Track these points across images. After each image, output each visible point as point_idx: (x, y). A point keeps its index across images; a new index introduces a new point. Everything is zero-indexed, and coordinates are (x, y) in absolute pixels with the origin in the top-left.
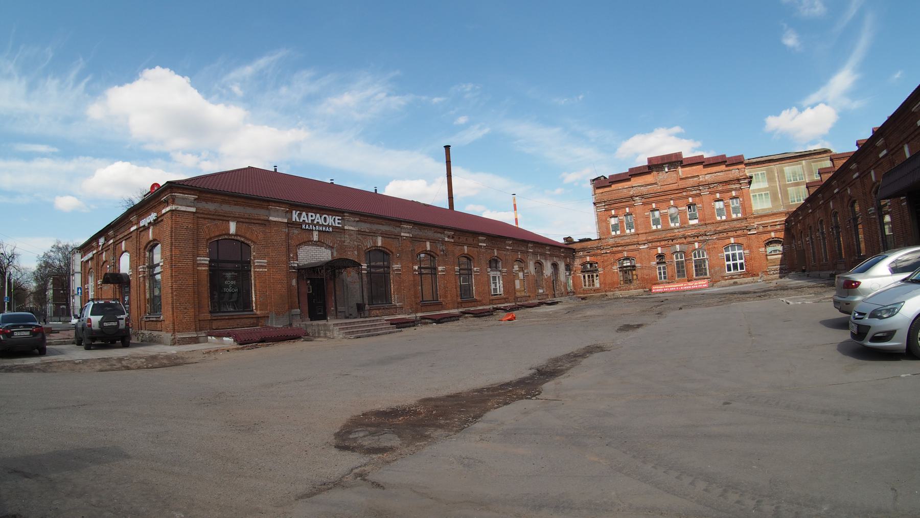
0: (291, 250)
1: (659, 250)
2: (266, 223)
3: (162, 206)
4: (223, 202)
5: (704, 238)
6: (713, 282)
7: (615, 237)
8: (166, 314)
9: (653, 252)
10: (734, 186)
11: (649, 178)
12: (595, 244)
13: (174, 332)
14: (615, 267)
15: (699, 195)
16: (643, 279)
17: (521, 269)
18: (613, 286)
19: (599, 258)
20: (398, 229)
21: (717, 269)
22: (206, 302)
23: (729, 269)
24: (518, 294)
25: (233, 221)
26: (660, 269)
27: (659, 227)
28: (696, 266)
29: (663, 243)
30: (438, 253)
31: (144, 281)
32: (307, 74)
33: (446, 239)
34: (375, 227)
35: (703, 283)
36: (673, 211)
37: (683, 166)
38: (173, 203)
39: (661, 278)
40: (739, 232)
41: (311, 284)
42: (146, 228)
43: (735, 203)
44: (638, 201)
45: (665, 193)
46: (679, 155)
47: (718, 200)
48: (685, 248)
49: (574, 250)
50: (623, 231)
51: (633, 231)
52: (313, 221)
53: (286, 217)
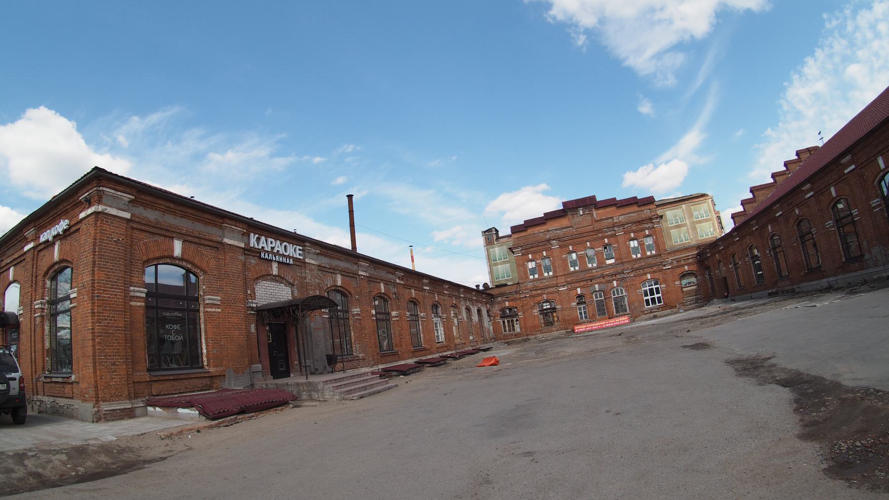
0: (248, 284)
1: (579, 291)
2: (218, 246)
3: (77, 210)
4: (168, 211)
5: (622, 276)
6: (633, 318)
7: (534, 280)
8: (83, 371)
9: (573, 293)
10: (647, 226)
11: (564, 222)
12: (514, 289)
13: (97, 402)
14: (535, 311)
15: (614, 236)
16: (565, 320)
17: (456, 315)
18: (535, 329)
19: (518, 302)
20: (355, 267)
21: (636, 304)
22: (142, 354)
23: (648, 304)
24: (457, 341)
25: (179, 239)
26: (580, 309)
27: (577, 268)
28: (616, 304)
29: (582, 284)
30: (391, 296)
31: (42, 322)
32: (197, 132)
33: (398, 281)
34: (335, 263)
35: (624, 319)
36: (590, 252)
37: (597, 208)
38: (100, 202)
39: (582, 318)
40: (655, 268)
41: (271, 330)
42: (49, 244)
43: (649, 241)
44: (555, 245)
45: (582, 235)
46: (593, 198)
47: (633, 239)
48: (603, 286)
49: (492, 296)
50: (541, 274)
51: (551, 273)
52: (273, 248)
53: (242, 241)
